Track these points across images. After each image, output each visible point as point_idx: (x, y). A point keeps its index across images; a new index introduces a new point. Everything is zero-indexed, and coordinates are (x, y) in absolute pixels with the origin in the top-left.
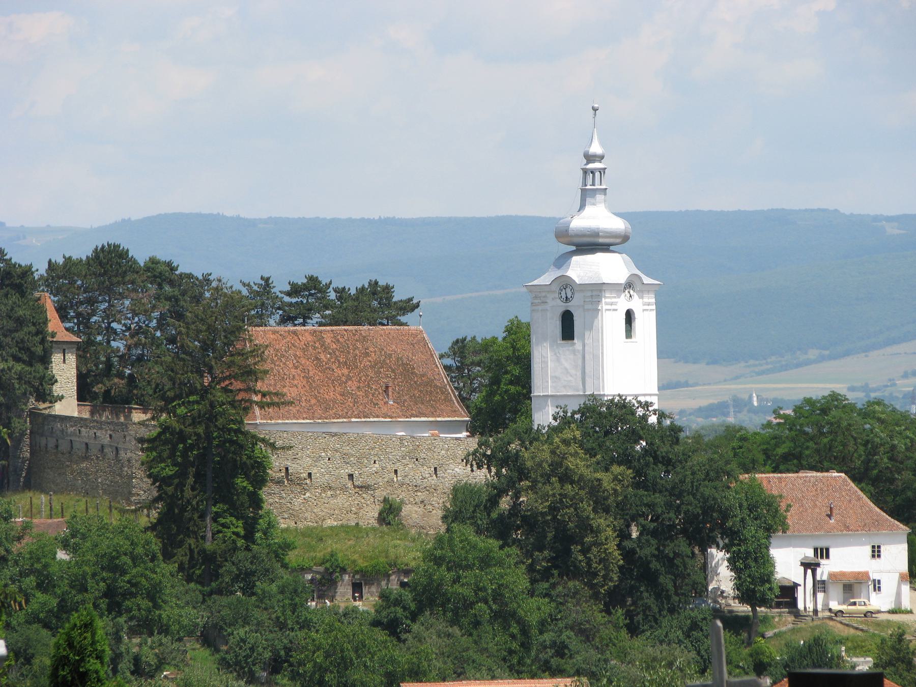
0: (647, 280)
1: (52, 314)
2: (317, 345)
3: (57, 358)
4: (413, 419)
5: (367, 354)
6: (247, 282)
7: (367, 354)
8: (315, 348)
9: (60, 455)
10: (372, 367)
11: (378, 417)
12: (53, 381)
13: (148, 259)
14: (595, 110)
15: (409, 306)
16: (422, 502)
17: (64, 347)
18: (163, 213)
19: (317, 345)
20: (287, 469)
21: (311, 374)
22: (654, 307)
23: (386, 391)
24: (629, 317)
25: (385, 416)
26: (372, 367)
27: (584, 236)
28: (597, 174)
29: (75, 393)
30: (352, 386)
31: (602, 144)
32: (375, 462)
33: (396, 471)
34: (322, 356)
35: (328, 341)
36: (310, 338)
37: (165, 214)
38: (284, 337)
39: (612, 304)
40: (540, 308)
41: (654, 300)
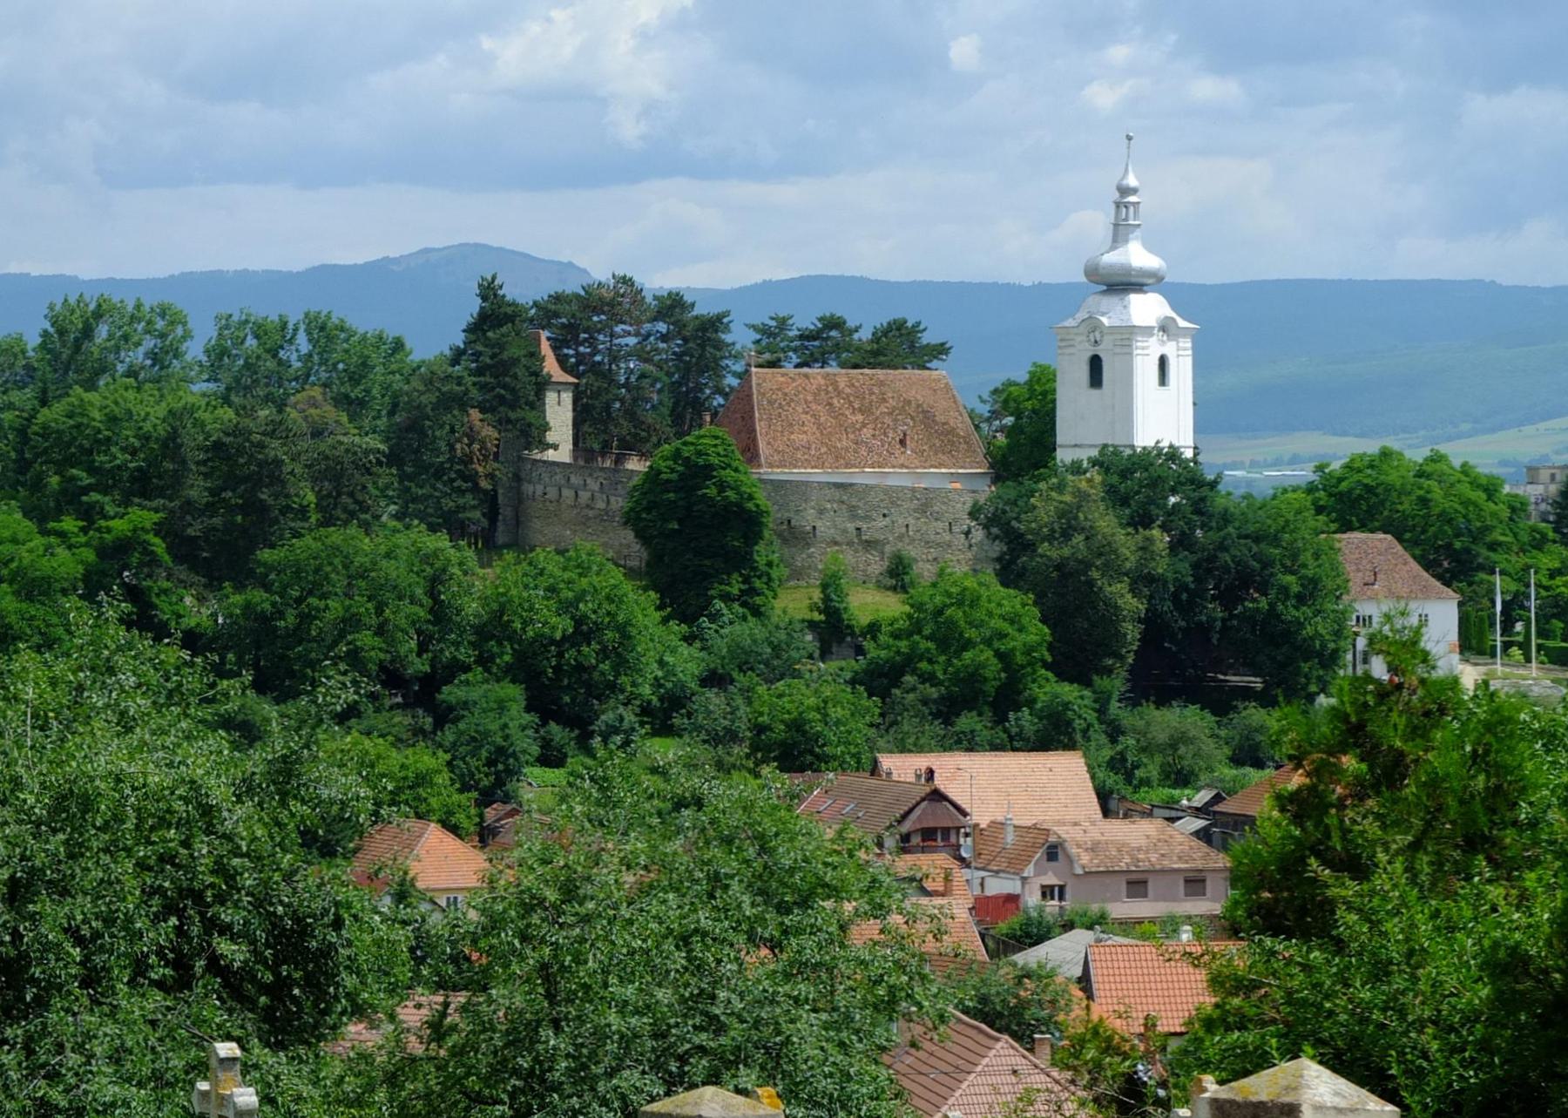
0: (1182, 323)
1: (546, 348)
2: (830, 388)
3: (551, 397)
4: (932, 470)
5: (884, 400)
6: (757, 322)
7: (884, 400)
8: (827, 392)
9: (548, 504)
10: (890, 414)
11: (894, 467)
12: (546, 427)
13: (1165, 444)
14: (1129, 138)
15: (940, 350)
16: (935, 559)
17: (560, 388)
18: (176, 273)
19: (830, 388)
20: (789, 522)
21: (822, 419)
22: (1190, 352)
23: (903, 442)
24: (1163, 362)
25: (902, 466)
26: (890, 414)
27: (1119, 275)
28: (1131, 209)
29: (571, 438)
30: (867, 433)
31: (1137, 177)
32: (884, 515)
33: (907, 526)
34: (835, 401)
35: (842, 385)
36: (823, 382)
37: (182, 274)
38: (793, 380)
39: (1143, 348)
40: (1068, 351)
41: (1189, 345)
